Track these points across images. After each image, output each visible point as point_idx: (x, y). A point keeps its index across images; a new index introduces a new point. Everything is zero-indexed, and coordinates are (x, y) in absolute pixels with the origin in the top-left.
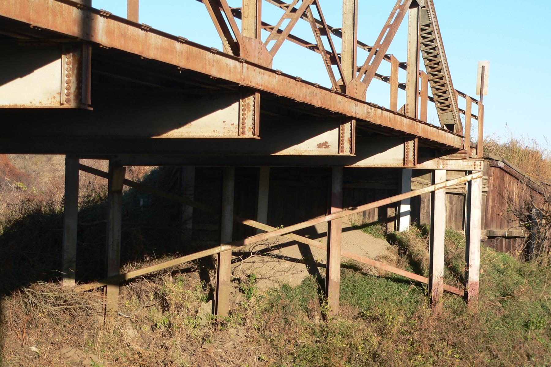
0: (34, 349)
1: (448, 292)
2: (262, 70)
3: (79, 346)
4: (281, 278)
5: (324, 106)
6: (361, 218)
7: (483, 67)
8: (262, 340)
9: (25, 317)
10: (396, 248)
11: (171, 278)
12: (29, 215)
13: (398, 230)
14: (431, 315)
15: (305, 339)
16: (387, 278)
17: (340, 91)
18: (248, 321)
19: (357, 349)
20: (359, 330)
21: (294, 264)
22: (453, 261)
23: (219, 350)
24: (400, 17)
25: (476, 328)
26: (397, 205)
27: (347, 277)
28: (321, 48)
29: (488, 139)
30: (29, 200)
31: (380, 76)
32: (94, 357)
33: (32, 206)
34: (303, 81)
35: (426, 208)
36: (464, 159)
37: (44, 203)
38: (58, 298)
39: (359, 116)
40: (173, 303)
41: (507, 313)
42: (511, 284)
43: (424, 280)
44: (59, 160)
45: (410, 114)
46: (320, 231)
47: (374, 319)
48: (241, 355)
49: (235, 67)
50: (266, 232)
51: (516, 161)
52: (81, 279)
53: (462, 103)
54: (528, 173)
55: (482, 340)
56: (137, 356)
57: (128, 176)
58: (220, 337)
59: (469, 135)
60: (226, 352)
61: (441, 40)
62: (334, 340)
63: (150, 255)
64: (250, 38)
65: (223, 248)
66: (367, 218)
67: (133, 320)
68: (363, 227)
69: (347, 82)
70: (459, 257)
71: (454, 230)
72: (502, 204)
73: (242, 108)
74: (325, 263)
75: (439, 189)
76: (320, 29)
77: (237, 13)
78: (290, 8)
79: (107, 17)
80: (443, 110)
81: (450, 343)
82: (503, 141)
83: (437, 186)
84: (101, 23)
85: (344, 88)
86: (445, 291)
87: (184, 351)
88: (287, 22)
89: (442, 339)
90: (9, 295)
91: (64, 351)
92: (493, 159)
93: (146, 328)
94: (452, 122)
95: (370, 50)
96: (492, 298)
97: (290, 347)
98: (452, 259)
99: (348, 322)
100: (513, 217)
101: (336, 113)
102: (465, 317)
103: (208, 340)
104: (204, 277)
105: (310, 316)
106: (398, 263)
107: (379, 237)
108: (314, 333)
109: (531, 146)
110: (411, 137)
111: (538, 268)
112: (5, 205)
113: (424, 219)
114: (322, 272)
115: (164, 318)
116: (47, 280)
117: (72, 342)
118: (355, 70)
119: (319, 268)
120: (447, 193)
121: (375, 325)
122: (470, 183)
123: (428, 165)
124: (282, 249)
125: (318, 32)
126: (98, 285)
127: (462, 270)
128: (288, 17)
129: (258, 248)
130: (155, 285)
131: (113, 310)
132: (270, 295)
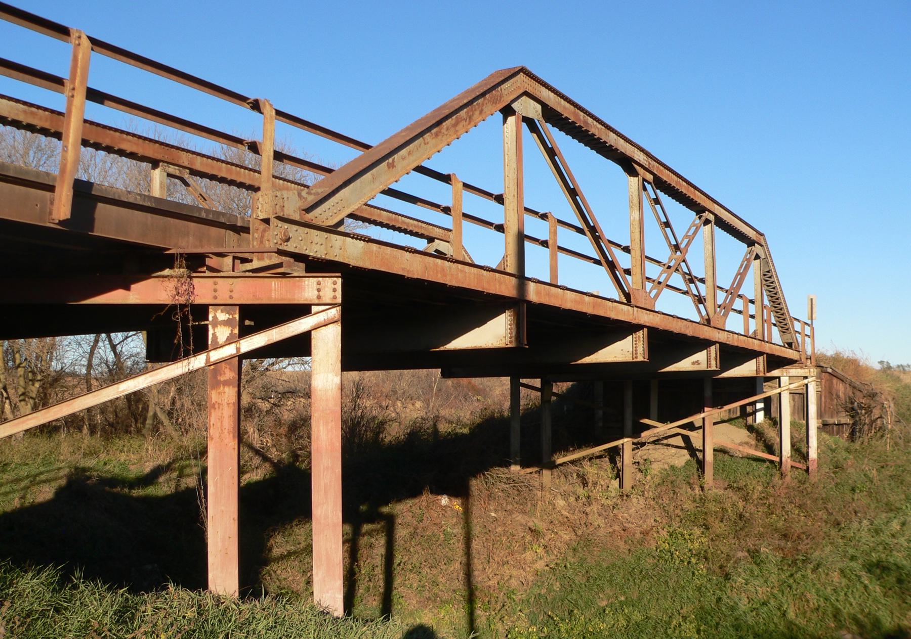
0: (493, 514)
1: (794, 467)
2: (648, 312)
3: (525, 513)
4: (669, 461)
5: (695, 335)
6: (728, 414)
7: (812, 300)
8: (657, 507)
9: (486, 492)
10: (754, 435)
11: (588, 463)
12: (486, 420)
13: (755, 422)
14: (782, 485)
15: (688, 505)
16: (748, 459)
17: (706, 323)
18: (646, 493)
19: (727, 511)
20: (728, 498)
21: (679, 450)
22: (798, 444)
23: (626, 515)
24: (747, 267)
25: (816, 493)
26: (753, 404)
27: (718, 458)
28: (690, 293)
29: (819, 352)
30: (486, 409)
31: (735, 310)
32: (536, 521)
33: (488, 413)
34: (678, 318)
35: (775, 405)
36: (801, 368)
37: (497, 411)
38: (508, 479)
39: (721, 341)
40: (590, 481)
41: (839, 481)
42: (841, 459)
43: (775, 459)
44: (506, 380)
45: (760, 337)
46: (697, 425)
47: (739, 489)
48: (641, 518)
49: (628, 311)
50: (657, 427)
51: (840, 368)
52: (524, 465)
53: (798, 326)
54: (849, 376)
55: (821, 501)
56: (566, 520)
57: (555, 390)
58: (626, 505)
59: (805, 350)
60: (630, 516)
61: (779, 282)
62: (710, 506)
63: (573, 446)
64: (638, 290)
65: (626, 440)
67: (562, 494)
68: (729, 421)
69: (711, 316)
70: (801, 440)
71: (797, 420)
72: (832, 400)
73: (634, 339)
74: (702, 448)
75: (784, 390)
76: (689, 279)
77: (628, 272)
78: (666, 266)
79: (536, 283)
80: (784, 332)
81: (797, 505)
82: (830, 353)
83: (783, 389)
84: (532, 286)
85: (709, 320)
86: (792, 466)
87: (600, 515)
88: (664, 275)
89: (791, 502)
90: (475, 476)
91: (514, 516)
92: (823, 367)
93: (572, 499)
94: (791, 341)
95: (727, 291)
96: (827, 470)
97: (678, 511)
98: (797, 442)
99: (720, 492)
100: (841, 409)
101: (704, 340)
102: (807, 485)
103: (617, 508)
104: (613, 461)
105: (693, 489)
107: (741, 428)
108: (695, 501)
109: (851, 356)
110: (761, 354)
111: (860, 447)
112: (470, 412)
113: (774, 414)
114: (700, 455)
115: (584, 492)
116: (501, 466)
117: (520, 511)
118: (717, 306)
119: (697, 452)
120: (790, 393)
121: (740, 494)
122: (807, 385)
123: (775, 373)
124: (669, 439)
125: (688, 282)
126: (536, 469)
127: (804, 450)
128: (665, 272)
129: (652, 439)
130: (577, 468)
131: (547, 487)
132: (662, 473)
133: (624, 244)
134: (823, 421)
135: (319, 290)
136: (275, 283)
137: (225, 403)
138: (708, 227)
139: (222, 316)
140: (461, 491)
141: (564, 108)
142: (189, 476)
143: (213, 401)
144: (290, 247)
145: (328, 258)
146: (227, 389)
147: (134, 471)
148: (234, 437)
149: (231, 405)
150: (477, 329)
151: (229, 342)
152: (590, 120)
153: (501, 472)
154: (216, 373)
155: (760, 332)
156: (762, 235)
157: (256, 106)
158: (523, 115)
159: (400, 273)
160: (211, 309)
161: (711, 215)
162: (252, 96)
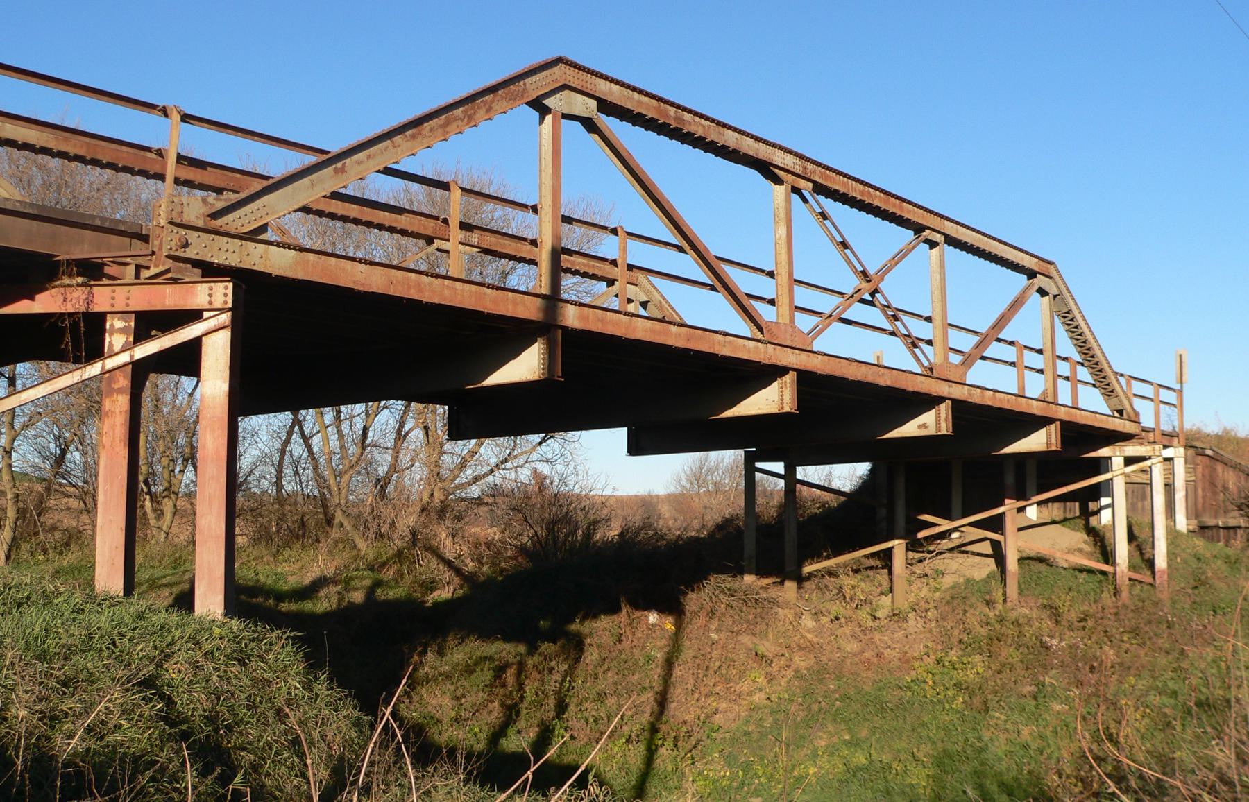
7: (1181, 356)
10: (1090, 540)
28: (898, 334)
36: (1141, 444)
52: (761, 572)
65: (897, 542)
66: (1068, 512)
72: (1215, 493)
82: (1212, 427)
83: (1115, 474)
86: (1130, 579)
92: (1196, 447)
94: (1120, 408)
106: (1089, 556)
107: (1078, 530)
133: (768, 269)
134: (1199, 522)
135: (210, 295)
136: (169, 289)
137: (117, 411)
138: (936, 251)
139: (119, 324)
140: (672, 606)
141: (639, 102)
142: (356, 589)
143: (107, 409)
144: (190, 253)
145: (242, 266)
146: (120, 397)
147: (292, 582)
148: (125, 444)
149: (123, 413)
150: (512, 361)
151: (123, 351)
152: (688, 116)
153: (727, 581)
154: (110, 381)
155: (1050, 392)
156: (1051, 263)
157: (165, 112)
158: (563, 112)
159: (350, 286)
160: (109, 317)
161: (938, 235)
162: (161, 104)
